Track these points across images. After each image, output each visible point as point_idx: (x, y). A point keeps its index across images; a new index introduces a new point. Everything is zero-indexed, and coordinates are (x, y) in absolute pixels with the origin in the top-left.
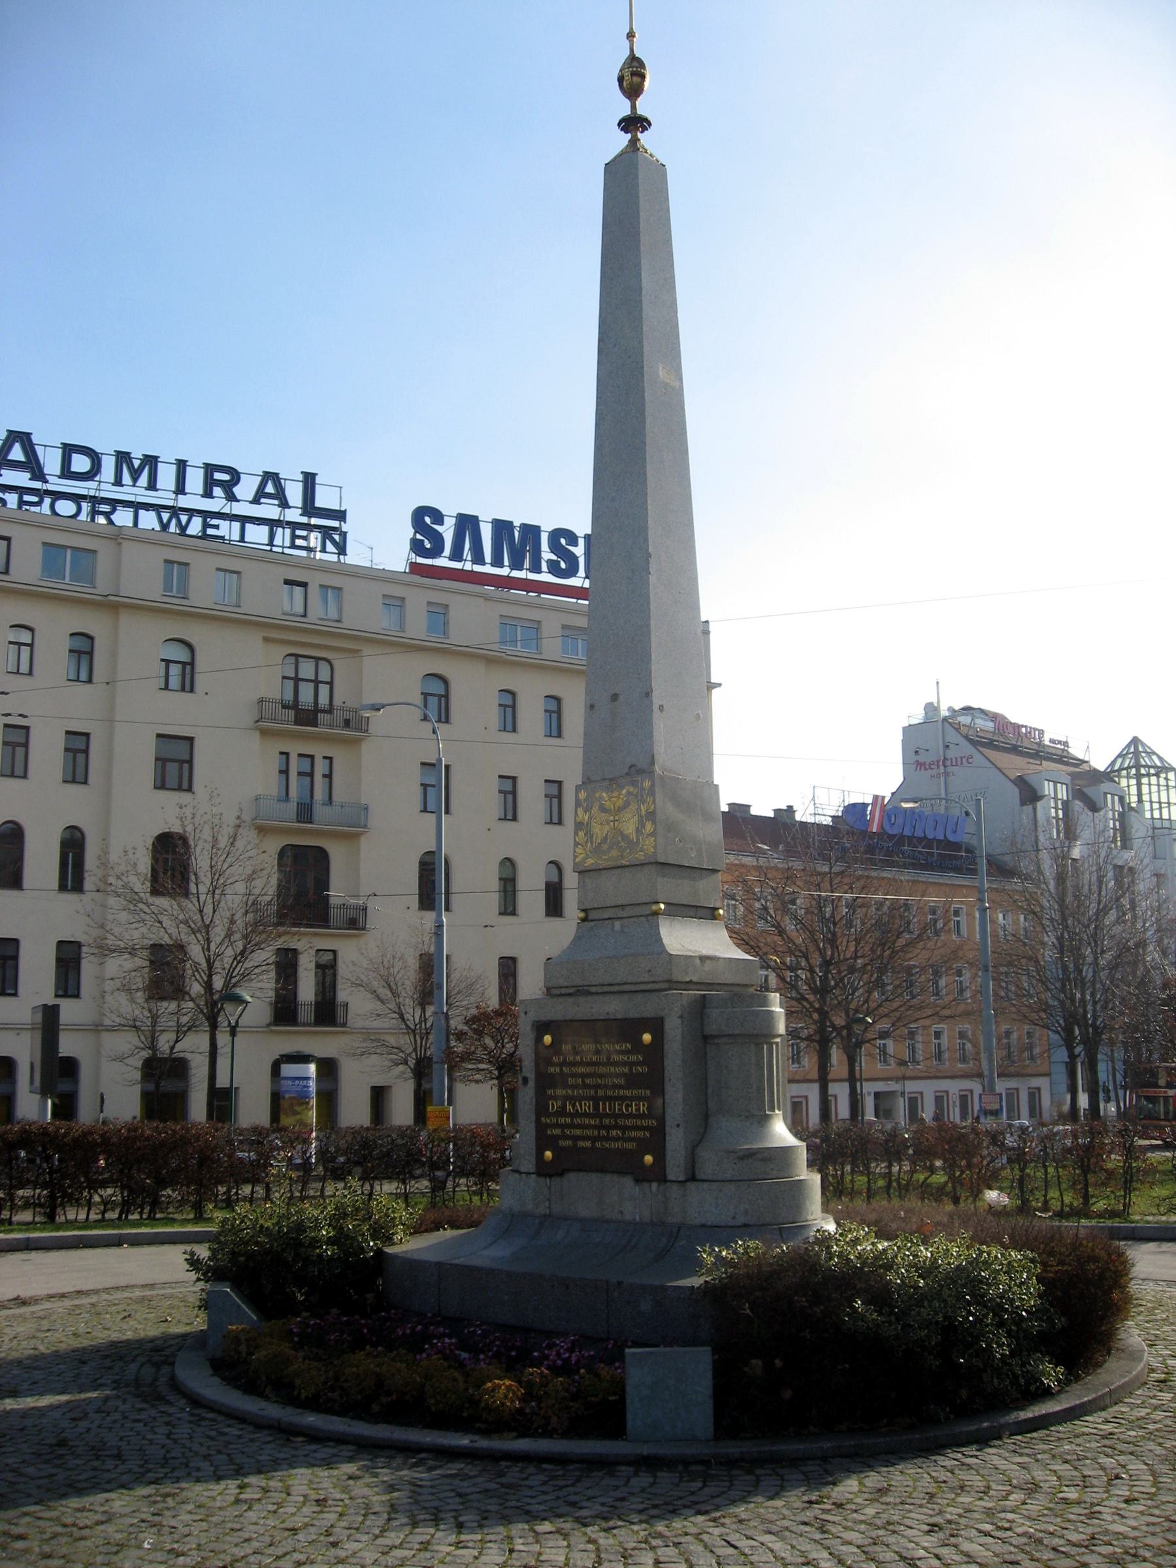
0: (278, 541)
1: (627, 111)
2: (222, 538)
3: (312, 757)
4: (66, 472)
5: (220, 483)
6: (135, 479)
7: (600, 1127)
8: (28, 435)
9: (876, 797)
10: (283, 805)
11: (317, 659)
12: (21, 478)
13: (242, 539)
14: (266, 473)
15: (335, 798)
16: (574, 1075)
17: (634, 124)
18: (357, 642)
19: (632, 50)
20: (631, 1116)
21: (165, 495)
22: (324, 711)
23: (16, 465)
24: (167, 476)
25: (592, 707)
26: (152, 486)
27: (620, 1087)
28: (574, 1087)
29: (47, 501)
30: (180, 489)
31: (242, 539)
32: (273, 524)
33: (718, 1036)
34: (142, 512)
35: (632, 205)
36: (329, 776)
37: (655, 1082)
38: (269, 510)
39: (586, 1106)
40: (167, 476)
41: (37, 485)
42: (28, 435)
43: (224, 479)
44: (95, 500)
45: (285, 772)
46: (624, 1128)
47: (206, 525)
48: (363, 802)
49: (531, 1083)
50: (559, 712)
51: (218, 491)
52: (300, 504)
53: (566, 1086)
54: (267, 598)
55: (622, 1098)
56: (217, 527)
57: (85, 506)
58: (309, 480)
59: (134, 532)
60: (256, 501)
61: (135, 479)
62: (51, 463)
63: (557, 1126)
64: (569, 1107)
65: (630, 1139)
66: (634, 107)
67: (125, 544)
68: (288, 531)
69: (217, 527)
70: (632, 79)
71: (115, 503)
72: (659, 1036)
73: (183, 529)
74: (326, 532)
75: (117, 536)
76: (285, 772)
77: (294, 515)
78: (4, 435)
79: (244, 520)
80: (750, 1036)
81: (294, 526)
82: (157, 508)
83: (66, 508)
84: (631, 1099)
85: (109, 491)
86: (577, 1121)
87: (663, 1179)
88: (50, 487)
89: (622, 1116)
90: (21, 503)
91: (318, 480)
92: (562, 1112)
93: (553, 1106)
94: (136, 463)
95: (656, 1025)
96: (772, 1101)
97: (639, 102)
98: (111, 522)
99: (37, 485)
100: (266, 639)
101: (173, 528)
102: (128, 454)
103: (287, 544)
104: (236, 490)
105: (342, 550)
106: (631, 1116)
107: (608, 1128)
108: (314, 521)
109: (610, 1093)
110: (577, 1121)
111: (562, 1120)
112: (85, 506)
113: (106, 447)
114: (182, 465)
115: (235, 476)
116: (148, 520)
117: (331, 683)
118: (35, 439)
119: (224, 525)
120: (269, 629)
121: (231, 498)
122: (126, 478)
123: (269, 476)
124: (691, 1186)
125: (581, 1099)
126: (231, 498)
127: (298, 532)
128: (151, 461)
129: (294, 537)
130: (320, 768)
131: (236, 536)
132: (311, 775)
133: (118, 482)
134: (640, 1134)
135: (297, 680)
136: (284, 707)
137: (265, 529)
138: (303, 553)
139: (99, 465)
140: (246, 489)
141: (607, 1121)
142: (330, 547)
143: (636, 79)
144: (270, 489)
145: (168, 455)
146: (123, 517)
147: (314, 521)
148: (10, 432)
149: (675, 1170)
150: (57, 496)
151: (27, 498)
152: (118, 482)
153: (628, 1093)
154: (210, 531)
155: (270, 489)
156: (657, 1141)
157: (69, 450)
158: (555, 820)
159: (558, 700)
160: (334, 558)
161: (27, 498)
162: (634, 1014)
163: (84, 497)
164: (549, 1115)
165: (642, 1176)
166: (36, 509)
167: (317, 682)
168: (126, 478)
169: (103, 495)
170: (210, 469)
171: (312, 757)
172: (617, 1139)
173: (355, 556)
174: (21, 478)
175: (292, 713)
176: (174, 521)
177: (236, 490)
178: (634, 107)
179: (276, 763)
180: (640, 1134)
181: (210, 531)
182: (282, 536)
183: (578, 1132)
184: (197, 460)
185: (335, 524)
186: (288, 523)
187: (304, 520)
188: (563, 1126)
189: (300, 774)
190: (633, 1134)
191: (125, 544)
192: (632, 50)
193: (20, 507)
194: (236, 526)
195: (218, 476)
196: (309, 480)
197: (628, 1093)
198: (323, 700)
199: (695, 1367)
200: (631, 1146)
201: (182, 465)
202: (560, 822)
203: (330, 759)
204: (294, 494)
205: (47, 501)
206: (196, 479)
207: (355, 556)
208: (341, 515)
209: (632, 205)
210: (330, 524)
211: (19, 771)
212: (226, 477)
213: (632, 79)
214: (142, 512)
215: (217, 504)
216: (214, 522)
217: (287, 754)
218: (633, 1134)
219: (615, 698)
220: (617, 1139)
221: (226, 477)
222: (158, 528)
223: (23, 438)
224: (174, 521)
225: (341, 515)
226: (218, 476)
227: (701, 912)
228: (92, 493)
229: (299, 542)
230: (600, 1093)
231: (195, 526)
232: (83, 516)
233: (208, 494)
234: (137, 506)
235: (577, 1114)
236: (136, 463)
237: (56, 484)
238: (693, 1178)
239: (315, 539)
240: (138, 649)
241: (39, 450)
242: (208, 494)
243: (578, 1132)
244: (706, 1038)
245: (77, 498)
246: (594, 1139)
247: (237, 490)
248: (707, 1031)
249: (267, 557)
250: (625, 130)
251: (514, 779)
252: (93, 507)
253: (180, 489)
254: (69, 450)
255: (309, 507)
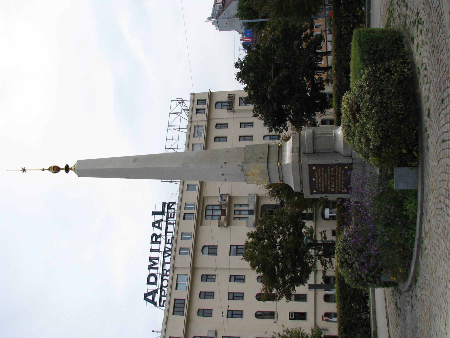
0: (172, 222)
1: (64, 171)
2: (172, 238)
3: (235, 210)
4: (155, 283)
5: (156, 239)
6: (156, 264)
7: (338, 179)
8: (145, 294)
9: (241, 40)
10: (249, 219)
11: (206, 210)
12: (157, 296)
13: (172, 232)
14: (153, 226)
15: (247, 203)
16: (324, 185)
17: (67, 169)
18: (201, 198)
19: (47, 170)
20: (335, 172)
21: (161, 255)
22: (221, 207)
23: (154, 298)
24: (155, 255)
25: (225, 180)
26: (158, 259)
27: (327, 174)
28: (328, 185)
29: (163, 288)
30: (158, 251)
31: (172, 232)
32: (167, 224)
33: (313, 150)
34: (166, 261)
35: (89, 169)
36: (240, 205)
37: (326, 167)
38: (163, 225)
39: (333, 182)
40: (155, 255)
41: (159, 291)
42: (145, 294)
43: (155, 239)
44: (163, 275)
45: (239, 218)
46: (338, 173)
47: (169, 243)
48: (247, 195)
49: (327, 195)
50: (219, 138)
51: (158, 240)
52: (161, 216)
53: (327, 187)
54: (189, 226)
55: (330, 173)
56: (169, 240)
57: (165, 278)
58: (154, 213)
59: (172, 264)
60: (161, 229)
61: (156, 264)
62: (152, 288)
63: (338, 189)
64: (333, 186)
65: (341, 172)
66: (62, 169)
67: (175, 266)
68: (169, 219)
69: (169, 240)
70: (56, 169)
71: (163, 270)
72: (313, 165)
73: (170, 250)
74: (169, 208)
75: (174, 268)
76: (239, 218)
77: (164, 218)
78: (145, 301)
79: (166, 232)
80: (313, 141)
81: (168, 217)
82: (164, 257)
83: (165, 283)
84: (330, 172)
85: (160, 271)
86: (336, 184)
87: (352, 164)
88: (160, 287)
89: (335, 174)
90: (164, 296)
91: (154, 211)
92: (334, 188)
93: (332, 189)
94: (152, 263)
95: (310, 166)
96: (331, 134)
97: (61, 167)
98: (169, 270)
99: (159, 291)
100: (201, 225)
101: (170, 252)
102: (149, 266)
103: (173, 219)
104: (158, 235)
105: (174, 203)
106: (335, 172)
107: (338, 177)
108: (166, 210)
109: (329, 177)
110: (336, 184)
111: (336, 188)
112: (165, 278)
113: (147, 272)
114: (152, 250)
115: (154, 235)
116: (168, 260)
117: (213, 205)
118: (146, 292)
119: (168, 238)
120: (199, 224)
121: (160, 236)
122: (156, 266)
123: (154, 225)
124: (353, 157)
125: (330, 184)
126: (160, 236)
127: (169, 216)
128: (151, 259)
129: (171, 217)
130: (238, 208)
131: (171, 234)
132: (240, 210)
133: (157, 268)
134: (340, 169)
135: (213, 216)
136: (220, 219)
137: (169, 226)
138: (176, 214)
139: (153, 274)
140: (157, 232)
141: (336, 177)
142: (173, 207)
143: (55, 168)
144: (157, 225)
145: (149, 254)
146: (167, 267)
147: (166, 210)
148: (144, 299)
149: (350, 161)
150: (162, 286)
151: (163, 294)
152: (157, 268)
153: (329, 173)
154: (170, 242)
155: (157, 225)
156: (342, 166)
157: (149, 283)
158: (251, 138)
159: (216, 138)
160: (176, 205)
161: (163, 294)
162: (308, 171)
163: (162, 278)
164: (335, 191)
165: (351, 169)
166: (166, 292)
167: (213, 210)
168: (156, 266)
169: (161, 273)
170: (152, 242)
171: (235, 210)
172: (341, 175)
173: (175, 199)
174: (157, 296)
175: (222, 217)
176: (168, 252)
177: (158, 235)
178: (62, 169)
179: (237, 221)
180: (340, 169)
181: (170, 242)
182: (171, 221)
183: (340, 184)
184: (150, 246)
185: (166, 205)
186: (167, 219)
187: (166, 214)
188: (338, 187)
189: (240, 214)
190: (340, 171)
191: (175, 266)
192: (47, 170)
193: (166, 296)
194: (168, 234)
195: (154, 240)
196: (154, 213)
197: (329, 173)
198: (218, 208)
199: (399, 172)
200: (343, 171)
201: (152, 250)
202: (252, 123)
203: (235, 205)
204: (158, 217)
205: (163, 288)
206: (155, 246)
207: (175, 199)
208: (164, 204)
209: (89, 169)
210: (167, 207)
211: (242, 295)
212: (154, 237)
213: (56, 169)
214: (166, 261)
215: (162, 240)
216: (167, 240)
217: (234, 218)
218: (340, 171)
219: (223, 175)
220: (341, 175)
221: (154, 237)
222: (170, 257)
223: (146, 295)
224: (168, 252)
225: (164, 204)
226: (154, 240)
227: (280, 151)
228: (161, 276)
229: (172, 216)
230: (329, 179)
231: (169, 246)
232: (168, 278)
233: (159, 243)
234: (164, 263)
235: (335, 184)
236: (152, 263)
237: (159, 286)
238: (351, 156)
239: (171, 211)
240: (206, 262)
241: (149, 291)
242: (159, 243)
243: (340, 184)
244: (314, 152)
245: (162, 280)
246: (341, 180)
247: (158, 234)
248: (312, 152)
249: (177, 226)
250: (68, 171)
251: (241, 123)
252: (165, 275)
253: (158, 251)
254: (149, 283)
255: (162, 213)
